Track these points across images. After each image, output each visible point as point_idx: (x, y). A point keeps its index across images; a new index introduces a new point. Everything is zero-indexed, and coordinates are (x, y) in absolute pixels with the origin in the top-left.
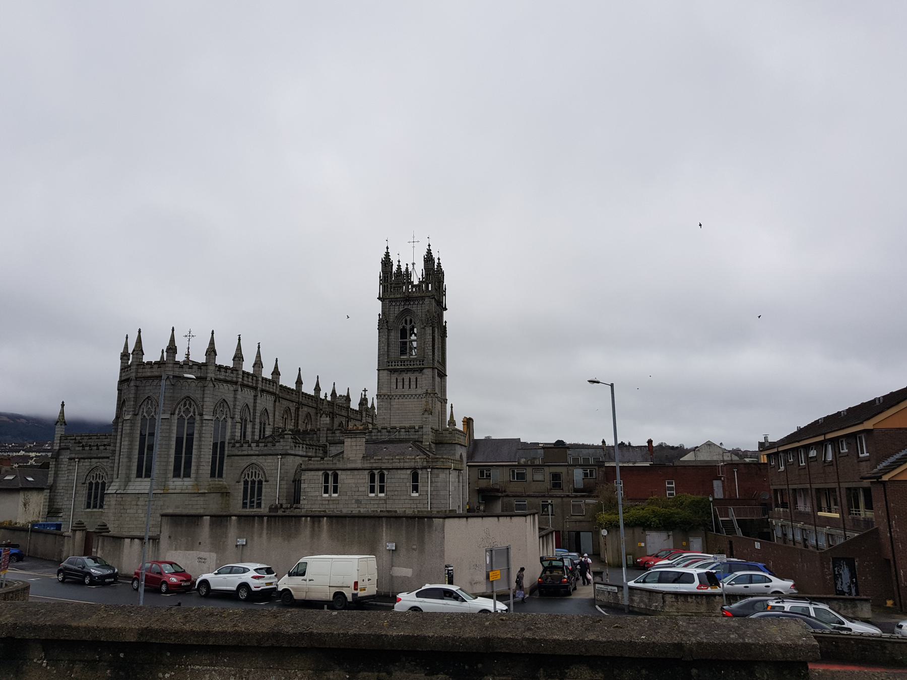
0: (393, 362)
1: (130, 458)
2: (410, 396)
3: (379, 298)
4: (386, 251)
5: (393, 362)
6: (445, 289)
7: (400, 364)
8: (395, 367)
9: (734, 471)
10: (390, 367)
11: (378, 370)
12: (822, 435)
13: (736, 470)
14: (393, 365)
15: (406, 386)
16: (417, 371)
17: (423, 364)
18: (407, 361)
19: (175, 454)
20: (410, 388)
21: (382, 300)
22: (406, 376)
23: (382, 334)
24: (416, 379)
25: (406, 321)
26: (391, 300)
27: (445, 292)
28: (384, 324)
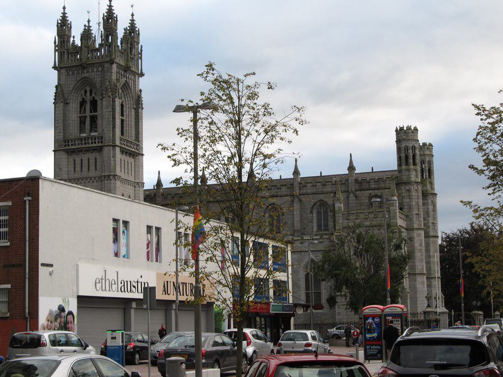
0: (83, 140)
1: (373, 310)
2: (93, 179)
3: (55, 68)
4: (131, 19)
5: (83, 140)
6: (141, 50)
7: (90, 141)
8: (79, 146)
9: (25, 201)
10: (67, 147)
11: (54, 151)
12: (376, 172)
13: (30, 198)
14: (70, 145)
15: (85, 168)
16: (97, 149)
17: (102, 142)
18: (78, 139)
19: (417, 307)
20: (75, 172)
21: (58, 69)
22: (85, 157)
23: (57, 109)
24: (82, 160)
25: (86, 92)
26: (68, 68)
27: (141, 54)
28: (61, 96)
